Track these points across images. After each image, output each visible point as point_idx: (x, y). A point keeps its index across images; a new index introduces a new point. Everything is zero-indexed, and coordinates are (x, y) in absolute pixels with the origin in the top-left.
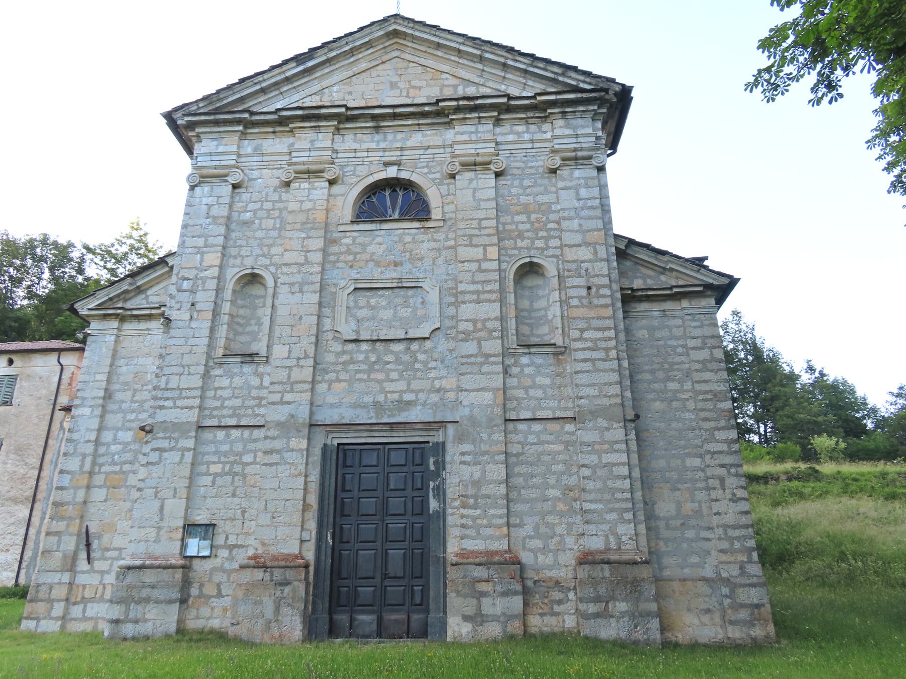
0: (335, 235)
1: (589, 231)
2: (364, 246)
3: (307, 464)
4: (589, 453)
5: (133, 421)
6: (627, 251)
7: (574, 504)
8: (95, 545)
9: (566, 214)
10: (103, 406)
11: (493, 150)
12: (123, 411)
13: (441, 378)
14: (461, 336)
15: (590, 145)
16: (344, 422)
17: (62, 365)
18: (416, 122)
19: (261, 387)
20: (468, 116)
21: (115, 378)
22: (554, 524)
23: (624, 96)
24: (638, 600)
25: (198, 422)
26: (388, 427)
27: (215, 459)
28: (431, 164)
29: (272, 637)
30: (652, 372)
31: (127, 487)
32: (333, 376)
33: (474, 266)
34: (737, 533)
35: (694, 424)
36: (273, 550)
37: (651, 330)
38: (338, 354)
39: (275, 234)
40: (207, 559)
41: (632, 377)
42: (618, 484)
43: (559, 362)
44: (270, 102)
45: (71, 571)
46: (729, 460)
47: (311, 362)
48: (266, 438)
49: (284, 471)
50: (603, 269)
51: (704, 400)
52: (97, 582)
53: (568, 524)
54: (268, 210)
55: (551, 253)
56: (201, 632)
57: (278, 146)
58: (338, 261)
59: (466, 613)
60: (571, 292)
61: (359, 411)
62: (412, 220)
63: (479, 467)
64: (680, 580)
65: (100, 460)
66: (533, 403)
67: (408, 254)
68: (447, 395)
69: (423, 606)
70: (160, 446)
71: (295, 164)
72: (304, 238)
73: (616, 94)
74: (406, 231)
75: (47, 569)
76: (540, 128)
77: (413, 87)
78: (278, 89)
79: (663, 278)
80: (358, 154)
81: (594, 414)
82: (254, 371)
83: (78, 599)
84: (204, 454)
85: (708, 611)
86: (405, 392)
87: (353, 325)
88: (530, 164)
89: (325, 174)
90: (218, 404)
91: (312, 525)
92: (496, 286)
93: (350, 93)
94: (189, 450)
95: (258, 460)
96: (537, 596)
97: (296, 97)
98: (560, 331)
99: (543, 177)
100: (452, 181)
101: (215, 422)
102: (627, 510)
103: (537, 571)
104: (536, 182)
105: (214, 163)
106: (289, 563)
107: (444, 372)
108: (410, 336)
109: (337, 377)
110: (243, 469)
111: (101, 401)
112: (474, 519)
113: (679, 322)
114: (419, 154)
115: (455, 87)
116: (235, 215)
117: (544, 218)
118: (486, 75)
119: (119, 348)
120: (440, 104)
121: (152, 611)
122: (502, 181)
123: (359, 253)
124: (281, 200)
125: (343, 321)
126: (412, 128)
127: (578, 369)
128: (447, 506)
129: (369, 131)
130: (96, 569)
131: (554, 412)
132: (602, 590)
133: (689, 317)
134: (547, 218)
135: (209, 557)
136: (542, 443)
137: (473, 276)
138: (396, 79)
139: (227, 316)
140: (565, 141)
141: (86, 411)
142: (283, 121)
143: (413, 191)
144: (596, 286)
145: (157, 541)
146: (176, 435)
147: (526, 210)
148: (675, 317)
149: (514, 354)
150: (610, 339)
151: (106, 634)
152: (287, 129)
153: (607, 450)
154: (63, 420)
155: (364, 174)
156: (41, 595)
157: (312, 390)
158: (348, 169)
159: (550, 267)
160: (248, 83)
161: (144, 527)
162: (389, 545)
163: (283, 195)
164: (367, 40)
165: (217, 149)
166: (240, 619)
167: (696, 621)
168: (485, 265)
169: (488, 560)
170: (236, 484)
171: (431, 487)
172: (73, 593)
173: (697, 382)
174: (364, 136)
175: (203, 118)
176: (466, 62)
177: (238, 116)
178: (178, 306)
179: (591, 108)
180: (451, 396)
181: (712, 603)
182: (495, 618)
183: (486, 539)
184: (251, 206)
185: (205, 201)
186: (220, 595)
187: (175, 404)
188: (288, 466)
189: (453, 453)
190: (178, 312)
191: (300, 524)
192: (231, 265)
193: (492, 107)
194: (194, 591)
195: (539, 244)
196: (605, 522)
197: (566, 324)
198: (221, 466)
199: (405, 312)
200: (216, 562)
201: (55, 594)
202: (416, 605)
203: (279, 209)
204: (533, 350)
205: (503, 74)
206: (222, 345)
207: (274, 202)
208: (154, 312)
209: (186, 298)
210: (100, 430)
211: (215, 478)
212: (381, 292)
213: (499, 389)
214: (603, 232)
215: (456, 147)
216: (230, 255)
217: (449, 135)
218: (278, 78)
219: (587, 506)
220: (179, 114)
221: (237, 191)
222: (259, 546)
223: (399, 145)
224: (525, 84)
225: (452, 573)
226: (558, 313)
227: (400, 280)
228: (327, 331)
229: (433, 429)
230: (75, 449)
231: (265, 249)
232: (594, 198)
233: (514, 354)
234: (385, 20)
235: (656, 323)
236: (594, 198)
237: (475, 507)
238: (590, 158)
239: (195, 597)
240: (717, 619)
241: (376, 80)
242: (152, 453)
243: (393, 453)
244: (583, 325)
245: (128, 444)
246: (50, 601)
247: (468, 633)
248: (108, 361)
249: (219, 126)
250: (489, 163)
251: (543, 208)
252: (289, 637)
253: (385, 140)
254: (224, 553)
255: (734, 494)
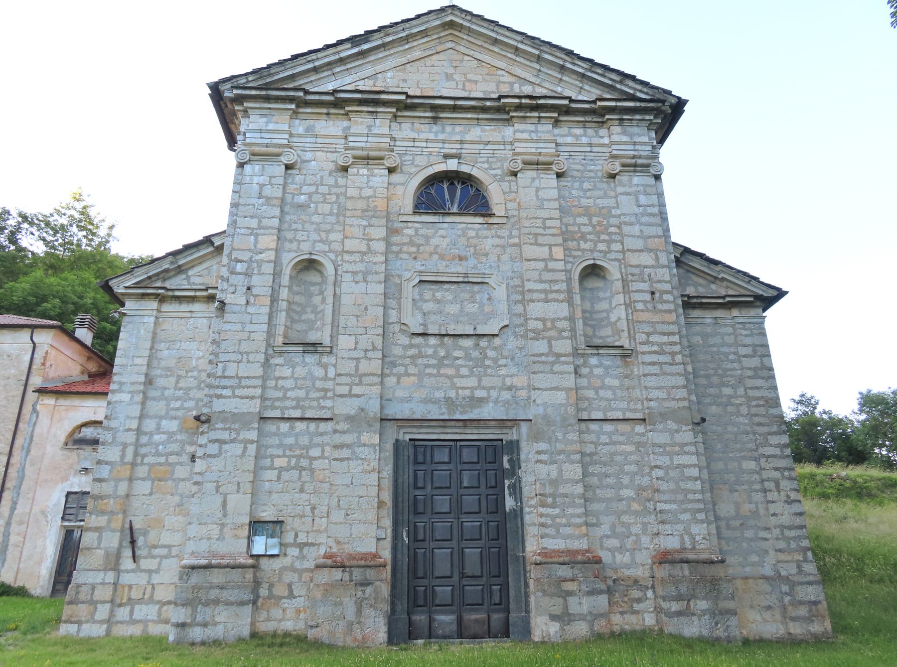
0: (397, 225)
1: (650, 237)
2: (427, 238)
3: (379, 460)
4: (661, 454)
5: (177, 409)
6: (685, 258)
7: (648, 504)
8: (140, 541)
9: (627, 219)
10: (144, 393)
11: (553, 151)
12: (166, 399)
13: (511, 376)
14: (531, 335)
15: (646, 153)
16: (415, 417)
17: (34, 343)
18: (476, 116)
19: (326, 378)
20: (528, 114)
21: (155, 363)
22: (630, 524)
23: (679, 106)
24: (717, 598)
25: (259, 412)
26: (461, 424)
27: (280, 452)
28: (490, 159)
29: (355, 639)
30: (708, 377)
31: (174, 480)
32: (401, 369)
33: (541, 265)
34: (792, 533)
35: (748, 428)
36: (348, 549)
37: (705, 336)
38: (405, 348)
39: (333, 219)
40: (276, 558)
41: (693, 379)
42: (690, 485)
43: (627, 365)
44: (322, 82)
45: (113, 569)
46: (782, 463)
47: (379, 354)
48: (335, 431)
49: (356, 467)
50: (666, 275)
51: (758, 406)
52: (144, 582)
53: (643, 524)
54: (324, 195)
55: (613, 257)
56: (274, 635)
57: (331, 128)
58: (401, 251)
59: (554, 613)
60: (636, 296)
61: (430, 407)
62: (475, 215)
63: (555, 466)
64: (742, 578)
65: (143, 451)
66: (603, 404)
67: (472, 249)
68: (519, 393)
69: (503, 604)
70: (219, 437)
71: (353, 149)
72: (365, 226)
73: (671, 106)
74: (469, 225)
75: (87, 567)
76: (597, 132)
77: (469, 81)
78: (331, 69)
79: (713, 286)
80: (417, 144)
81: (664, 416)
82: (317, 361)
83: (124, 601)
84: (267, 447)
85: (769, 608)
86: (476, 388)
87: (419, 318)
88: (589, 168)
89: (385, 162)
90: (280, 394)
91: (388, 523)
92: (564, 286)
93: (405, 81)
94: (252, 442)
95: (326, 454)
96: (617, 595)
97: (348, 80)
98: (626, 334)
99: (601, 181)
100: (514, 178)
101: (277, 414)
102: (699, 511)
103: (616, 570)
104: (595, 186)
105: (265, 141)
106: (369, 562)
107: (514, 370)
108: (478, 332)
109: (406, 371)
110: (311, 464)
111: (142, 387)
112: (554, 518)
113: (730, 330)
114: (480, 149)
115: (512, 84)
116: (289, 198)
117: (605, 222)
118: (542, 75)
119: (158, 331)
120: (502, 100)
121: (222, 614)
122: (563, 182)
123: (422, 245)
124: (336, 185)
125: (410, 313)
126: (471, 122)
127: (646, 372)
128: (524, 505)
129: (427, 121)
130: (143, 567)
131: (624, 414)
132: (683, 589)
133: (740, 326)
134: (608, 222)
135: (278, 555)
136: (615, 443)
137: (540, 275)
138: (451, 70)
139: (285, 303)
140: (623, 147)
141: (126, 397)
142: (339, 104)
143: (472, 186)
144: (659, 291)
145: (221, 538)
146: (237, 426)
147: (587, 212)
148: (726, 325)
149: (583, 355)
150: (675, 344)
151: (171, 638)
152: (342, 112)
153: (676, 452)
154: (37, 402)
155: (424, 164)
156: (82, 596)
157: (382, 383)
158: (407, 158)
159: (614, 271)
160: (301, 60)
161: (205, 524)
162: (465, 544)
163: (340, 179)
164: (423, 28)
165: (266, 126)
166: (320, 621)
167: (758, 618)
168: (551, 265)
169: (571, 559)
170: (304, 479)
171: (507, 485)
172: (118, 593)
173: (751, 388)
174: (422, 126)
175: (253, 92)
176: (522, 60)
177: (292, 93)
178: (232, 289)
179: (647, 117)
180: (523, 394)
181: (772, 600)
182: (582, 617)
183: (566, 537)
184: (305, 189)
185: (256, 180)
186: (291, 596)
187: (234, 393)
188: (360, 462)
189: (528, 451)
190: (232, 296)
191: (375, 522)
192: (286, 249)
193: (553, 108)
194: (264, 592)
195: (602, 247)
196: (679, 522)
197: (631, 327)
198: (286, 459)
199: (471, 308)
200: (286, 561)
201: (99, 594)
202: (495, 604)
203: (336, 194)
204: (601, 351)
205: (560, 76)
206: (281, 333)
207: (330, 186)
208: (198, 293)
209: (239, 280)
210: (142, 417)
211: (280, 472)
212: (446, 286)
213: (571, 389)
214: (663, 239)
215: (517, 144)
216: (286, 239)
217: (508, 132)
218: (332, 58)
219: (660, 506)
220: (228, 85)
221: (290, 172)
222: (334, 545)
223: (458, 138)
224: (581, 88)
225: (534, 573)
226: (624, 316)
227: (466, 275)
228: (393, 323)
229: (506, 427)
230: (114, 438)
231: (323, 235)
232: (653, 206)
233: (583, 355)
234: (443, 10)
235: (709, 330)
236: (653, 206)
237: (553, 506)
238: (648, 166)
239: (264, 599)
240: (778, 616)
241: (431, 70)
242: (210, 445)
243: (465, 451)
244: (648, 329)
245: (173, 433)
246: (93, 603)
247: (556, 632)
248: (148, 345)
249: (269, 103)
250: (551, 164)
251: (603, 211)
252: (373, 639)
253: (443, 131)
254: (294, 552)
255: (788, 496)
